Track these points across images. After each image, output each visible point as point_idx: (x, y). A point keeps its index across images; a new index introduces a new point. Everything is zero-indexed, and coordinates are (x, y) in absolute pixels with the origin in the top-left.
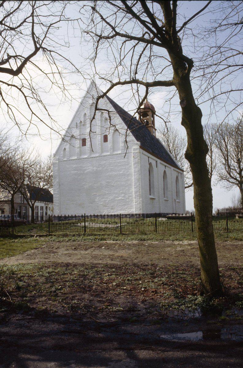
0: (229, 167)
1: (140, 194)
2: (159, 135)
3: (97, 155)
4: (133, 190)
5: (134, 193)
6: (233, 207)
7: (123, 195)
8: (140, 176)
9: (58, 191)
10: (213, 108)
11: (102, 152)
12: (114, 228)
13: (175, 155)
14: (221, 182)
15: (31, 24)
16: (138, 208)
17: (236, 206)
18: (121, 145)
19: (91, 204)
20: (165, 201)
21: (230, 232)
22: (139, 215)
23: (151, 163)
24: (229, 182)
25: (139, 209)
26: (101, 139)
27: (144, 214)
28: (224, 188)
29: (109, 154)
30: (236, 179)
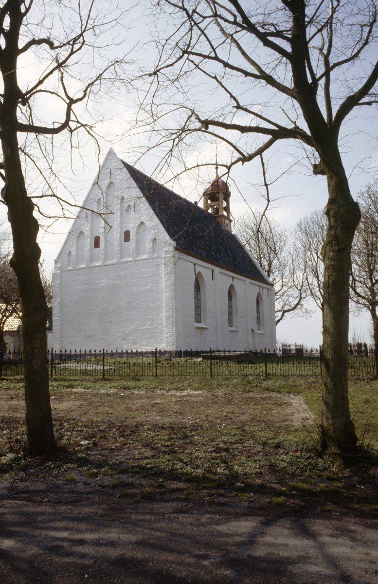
1: (172, 321)
2: (235, 229)
3: (115, 261)
4: (164, 314)
5: (164, 319)
7: (149, 322)
8: (173, 293)
9: (59, 317)
11: (122, 256)
12: (72, 372)
15: (203, 29)
18: (148, 245)
20: (231, 332)
23: (199, 272)
26: (120, 236)
29: (130, 259)
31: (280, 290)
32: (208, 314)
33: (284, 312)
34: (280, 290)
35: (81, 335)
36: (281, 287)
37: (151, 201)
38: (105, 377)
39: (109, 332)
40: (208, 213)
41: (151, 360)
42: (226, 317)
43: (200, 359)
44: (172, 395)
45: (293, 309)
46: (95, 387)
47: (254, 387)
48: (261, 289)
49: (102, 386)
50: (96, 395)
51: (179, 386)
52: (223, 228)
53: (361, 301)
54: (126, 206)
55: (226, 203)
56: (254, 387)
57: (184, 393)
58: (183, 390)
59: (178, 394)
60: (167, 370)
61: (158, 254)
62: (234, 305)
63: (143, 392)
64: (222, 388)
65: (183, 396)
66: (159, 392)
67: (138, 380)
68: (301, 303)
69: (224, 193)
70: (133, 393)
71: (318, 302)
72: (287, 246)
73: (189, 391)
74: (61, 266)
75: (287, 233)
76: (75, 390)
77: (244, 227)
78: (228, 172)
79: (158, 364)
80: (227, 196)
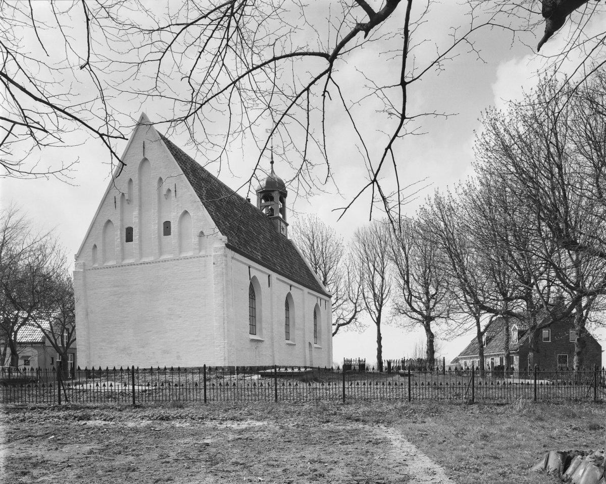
2: (292, 234)
10: (224, 47)
14: (397, 317)
18: (193, 240)
22: (223, 369)
25: (222, 358)
26: (159, 229)
27: (234, 367)
31: (335, 303)
32: (264, 325)
33: (340, 325)
34: (335, 303)
35: (111, 348)
36: (336, 300)
37: (198, 189)
38: (136, 403)
39: (147, 344)
40: (263, 214)
41: (197, 378)
43: (255, 377)
44: (229, 429)
45: (348, 323)
46: (120, 417)
47: (332, 414)
49: (131, 416)
50: (119, 432)
51: (236, 415)
53: (415, 315)
54: (164, 192)
56: (332, 414)
57: (244, 425)
58: (241, 420)
59: (235, 426)
60: (219, 391)
61: (206, 251)
63: (188, 424)
64: (292, 417)
65: (243, 430)
66: (209, 424)
67: (181, 407)
68: (356, 317)
69: (280, 193)
70: (173, 427)
71: (373, 316)
72: (344, 257)
73: (249, 421)
74: (84, 263)
75: (344, 244)
76: (90, 423)
77: (299, 234)
78: (329, 70)
79: (208, 383)
80: (283, 195)
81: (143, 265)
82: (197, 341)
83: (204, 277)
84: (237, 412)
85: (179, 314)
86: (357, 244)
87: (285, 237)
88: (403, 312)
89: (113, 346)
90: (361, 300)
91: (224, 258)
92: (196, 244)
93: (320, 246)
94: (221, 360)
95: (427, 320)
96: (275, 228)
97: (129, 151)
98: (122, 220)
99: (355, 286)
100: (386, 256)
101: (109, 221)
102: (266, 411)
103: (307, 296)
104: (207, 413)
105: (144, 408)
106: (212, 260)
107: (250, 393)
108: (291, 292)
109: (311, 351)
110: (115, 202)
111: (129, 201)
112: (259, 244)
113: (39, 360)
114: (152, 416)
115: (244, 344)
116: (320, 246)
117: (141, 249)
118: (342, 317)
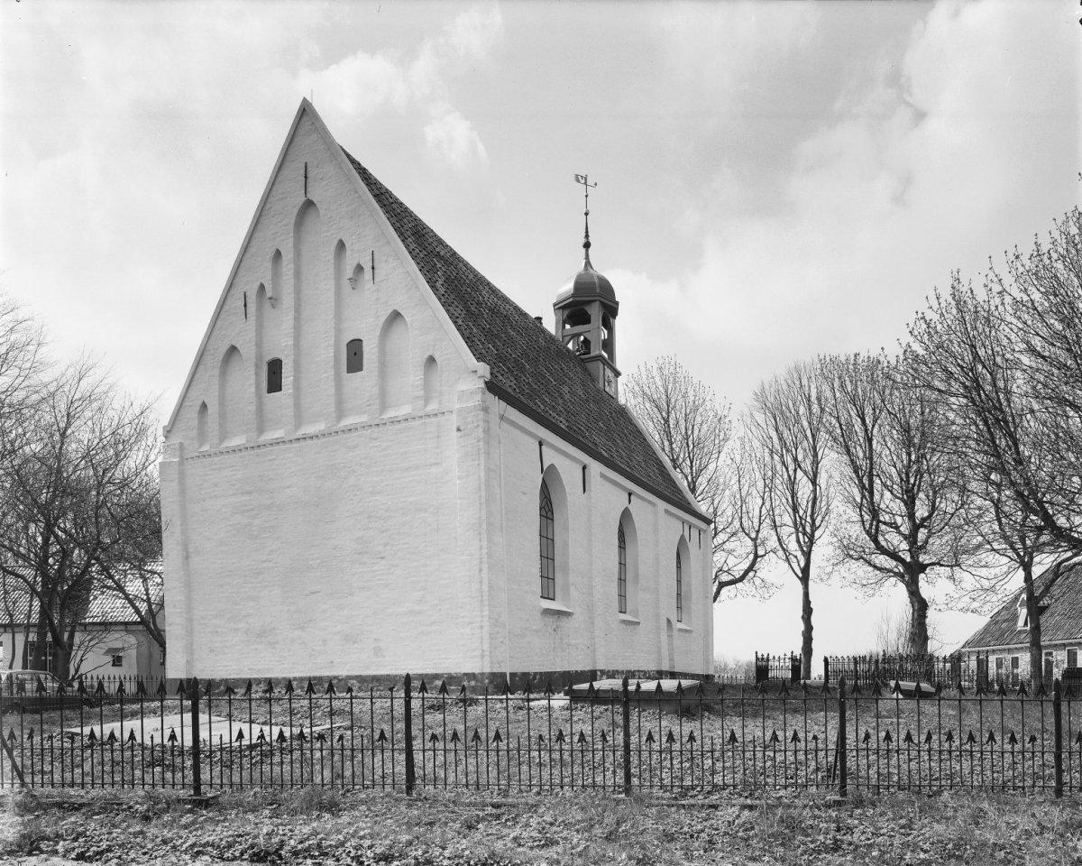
0: (875, 513)
2: (625, 392)
6: (882, 653)
13: (692, 479)
14: (842, 569)
16: (474, 651)
17: (891, 651)
19: (298, 633)
21: (859, 803)
23: (552, 467)
24: (871, 569)
28: (854, 585)
30: (894, 555)
32: (572, 578)
33: (722, 585)
35: (236, 630)
40: (568, 350)
42: (614, 589)
43: (559, 701)
45: (741, 579)
48: (687, 527)
52: (601, 385)
53: (882, 560)
54: (349, 271)
55: (606, 332)
61: (440, 403)
62: (629, 561)
67: (333, 808)
75: (733, 416)
77: (640, 399)
80: (610, 310)
81: (303, 443)
82: (419, 613)
83: (437, 464)
84: (505, 831)
85: (380, 552)
86: (760, 417)
87: (613, 398)
88: (856, 556)
89: (241, 625)
90: (766, 531)
91: (481, 415)
92: (417, 386)
93: (682, 423)
94: (475, 657)
95: (912, 572)
96: (594, 380)
97: (274, 189)
98: (259, 345)
99: (754, 504)
100: (823, 435)
101: (233, 349)
102: (598, 831)
103: (664, 520)
104: (405, 838)
105: (222, 809)
106: (454, 421)
107: (545, 756)
108: (630, 507)
109: (670, 636)
110: (245, 306)
111: (274, 301)
112: (561, 401)
113: (138, 654)
114: (230, 846)
115: (528, 620)
116: (682, 423)
117: (297, 405)
118: (725, 568)
